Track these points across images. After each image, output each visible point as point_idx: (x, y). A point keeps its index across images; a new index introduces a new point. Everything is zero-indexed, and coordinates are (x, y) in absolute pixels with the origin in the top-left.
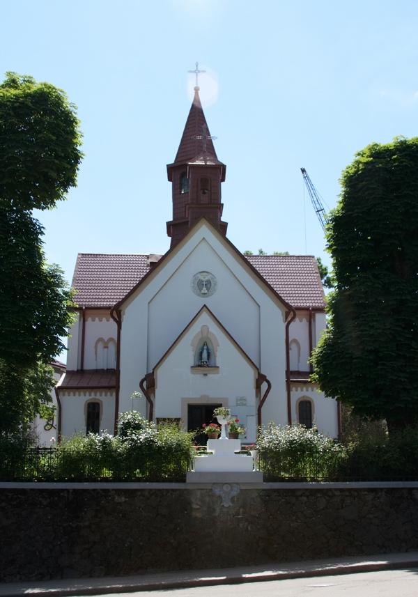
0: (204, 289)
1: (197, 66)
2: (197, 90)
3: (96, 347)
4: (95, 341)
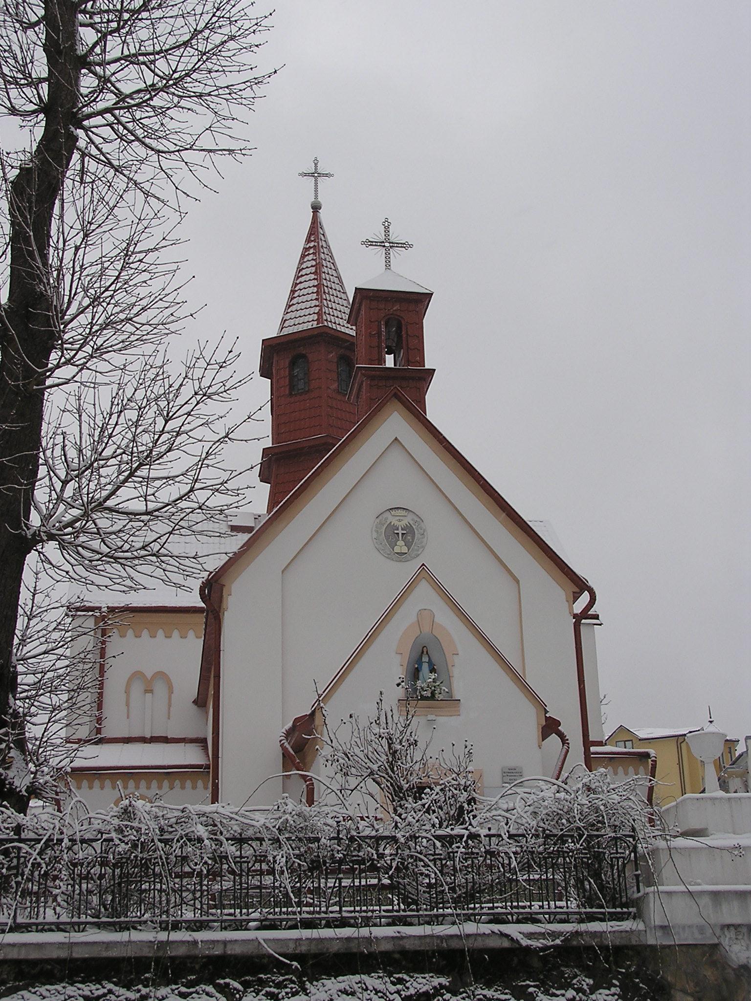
0: (401, 543)
1: (316, 164)
2: (316, 208)
3: (127, 692)
4: (128, 676)
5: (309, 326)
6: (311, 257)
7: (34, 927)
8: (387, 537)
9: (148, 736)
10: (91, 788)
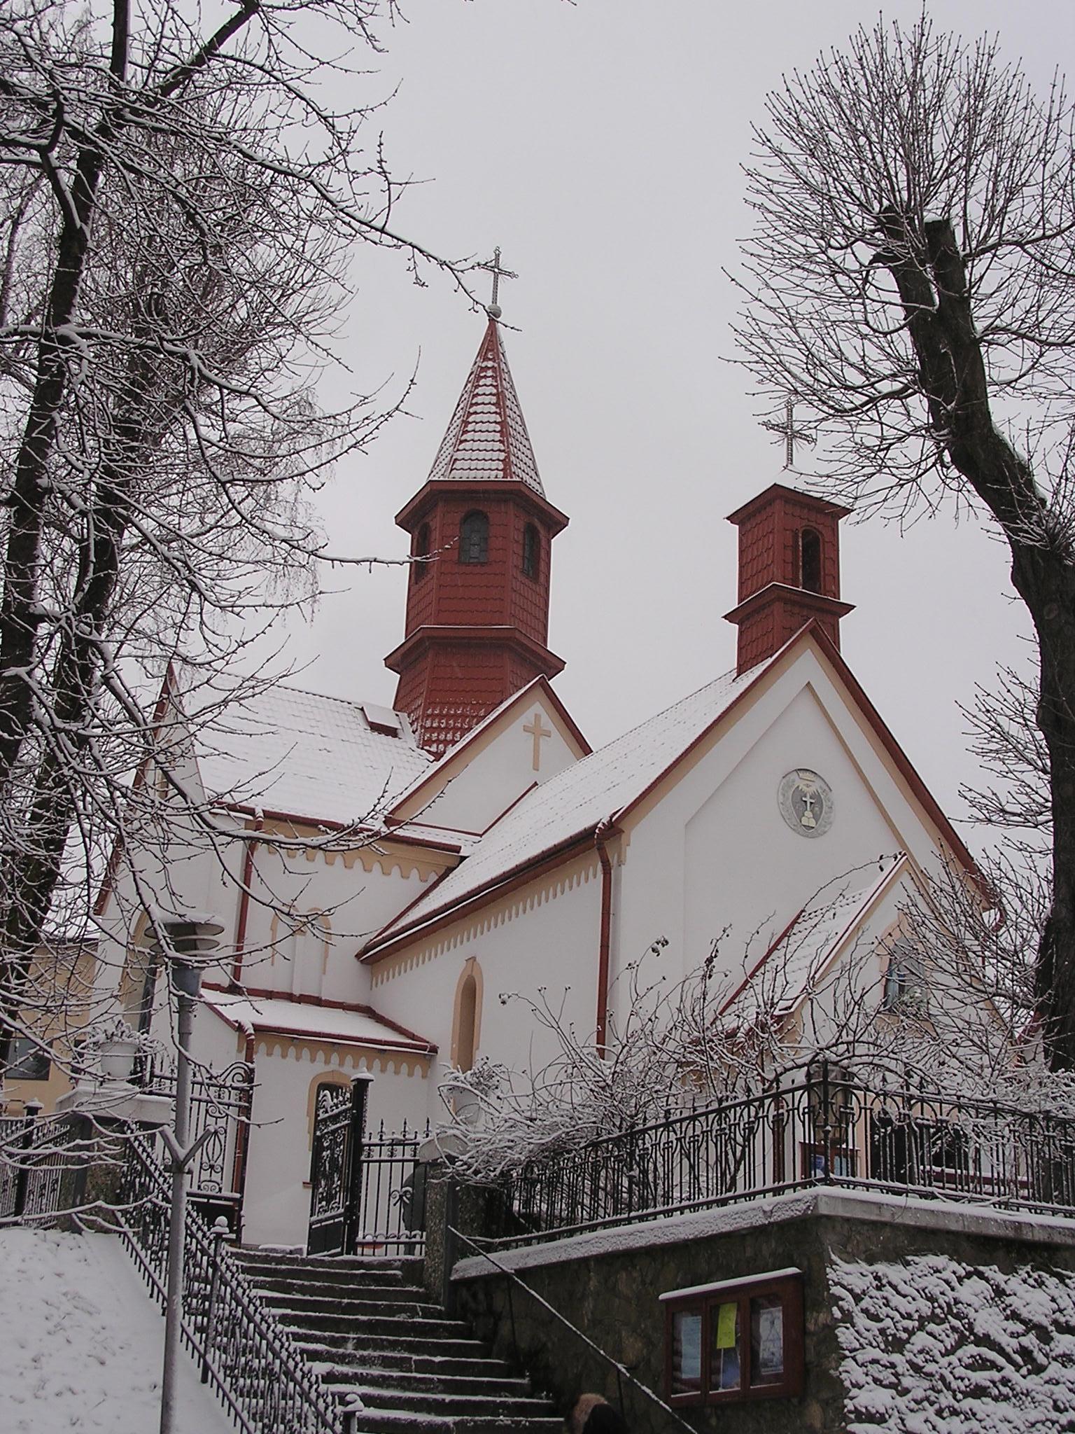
0: (808, 814)
5: (485, 475)
6: (489, 381)
7: (514, 1244)
9: (297, 992)
10: (284, 1056)
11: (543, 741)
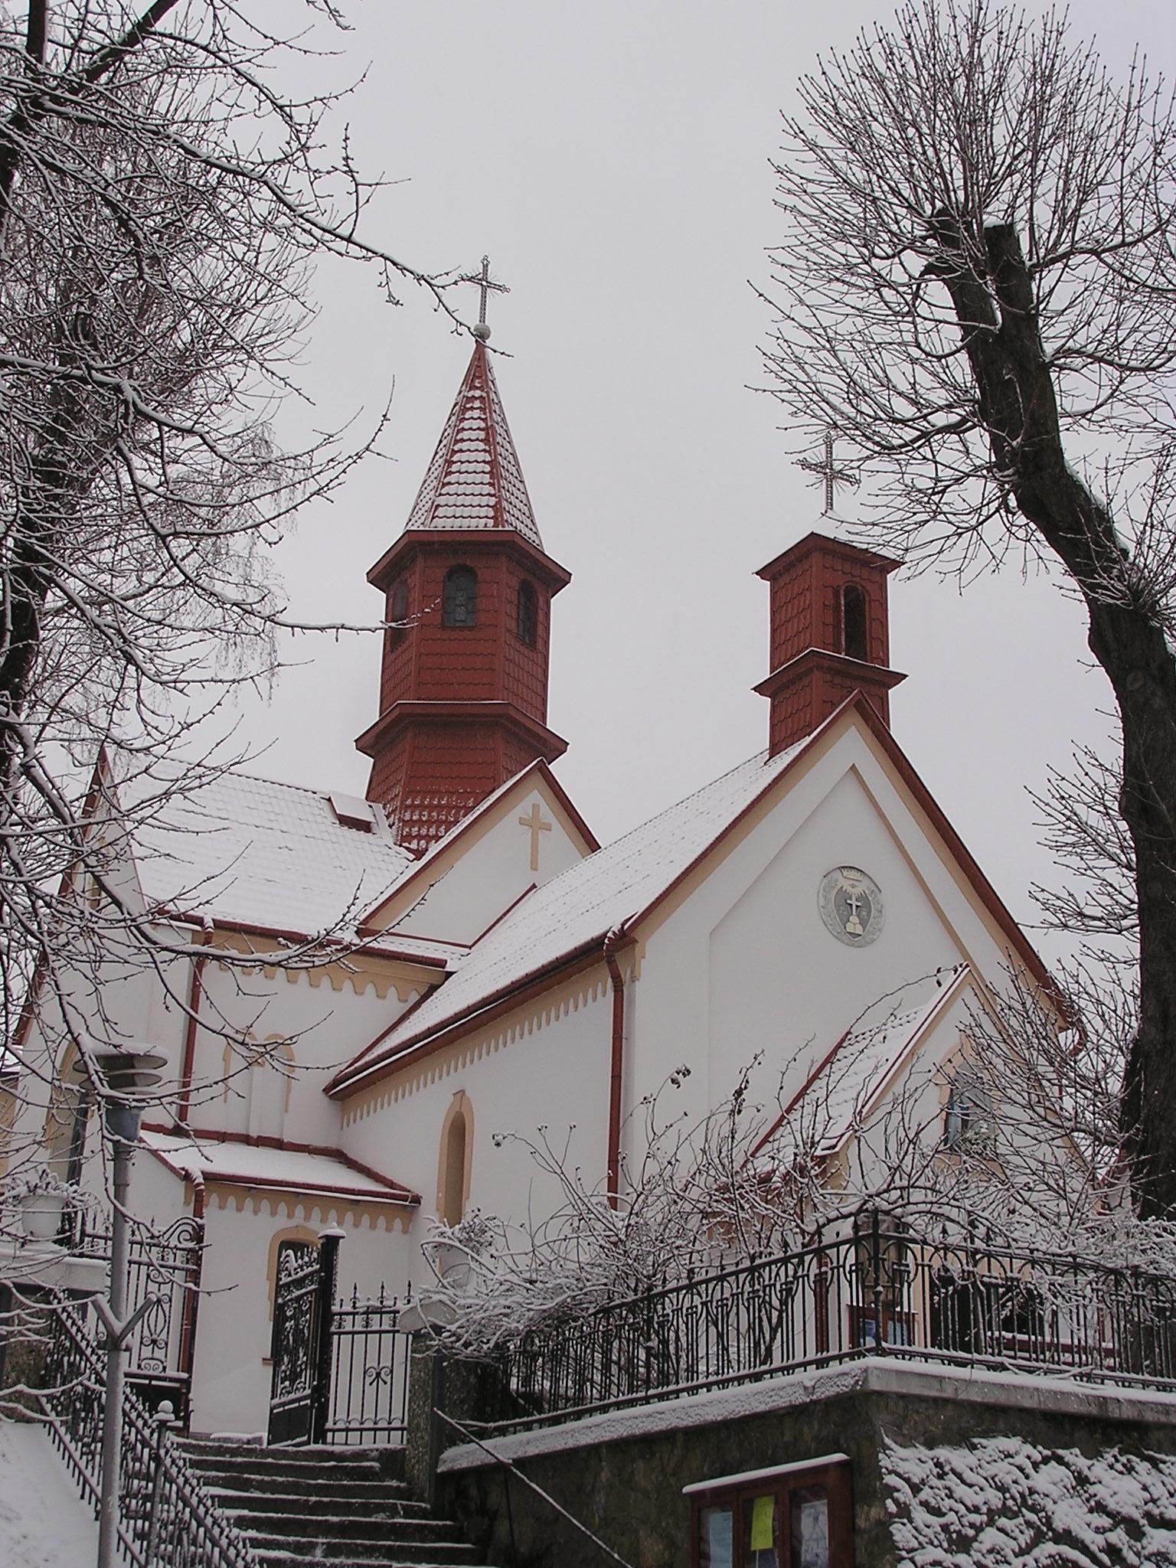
0: (854, 919)
8: (838, 907)
9: (254, 1134)
11: (541, 835)
